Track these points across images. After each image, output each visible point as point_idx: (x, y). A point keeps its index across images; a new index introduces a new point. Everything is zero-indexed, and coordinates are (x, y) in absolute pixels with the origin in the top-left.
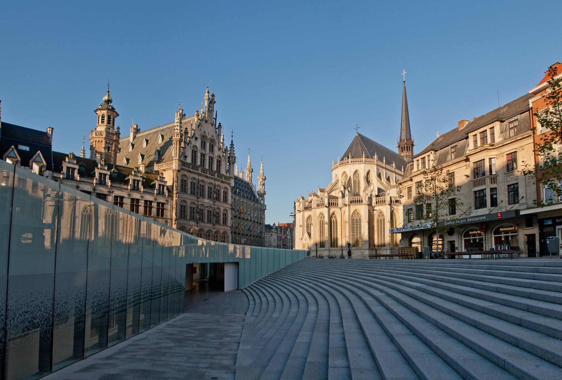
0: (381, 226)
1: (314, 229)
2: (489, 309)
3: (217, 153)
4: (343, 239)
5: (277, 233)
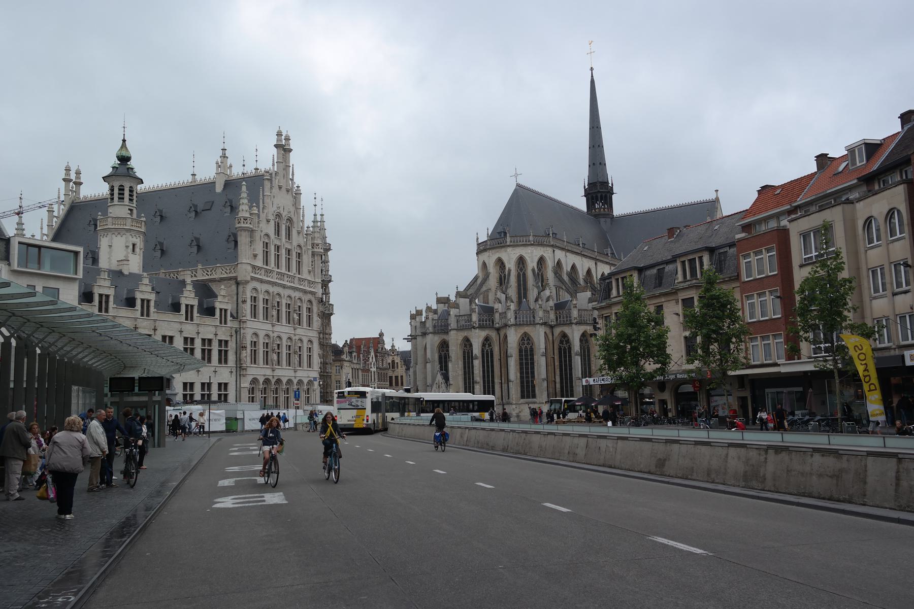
0: (565, 361)
2: (102, 425)
3: (296, 239)
4: (503, 385)
5: (350, 361)
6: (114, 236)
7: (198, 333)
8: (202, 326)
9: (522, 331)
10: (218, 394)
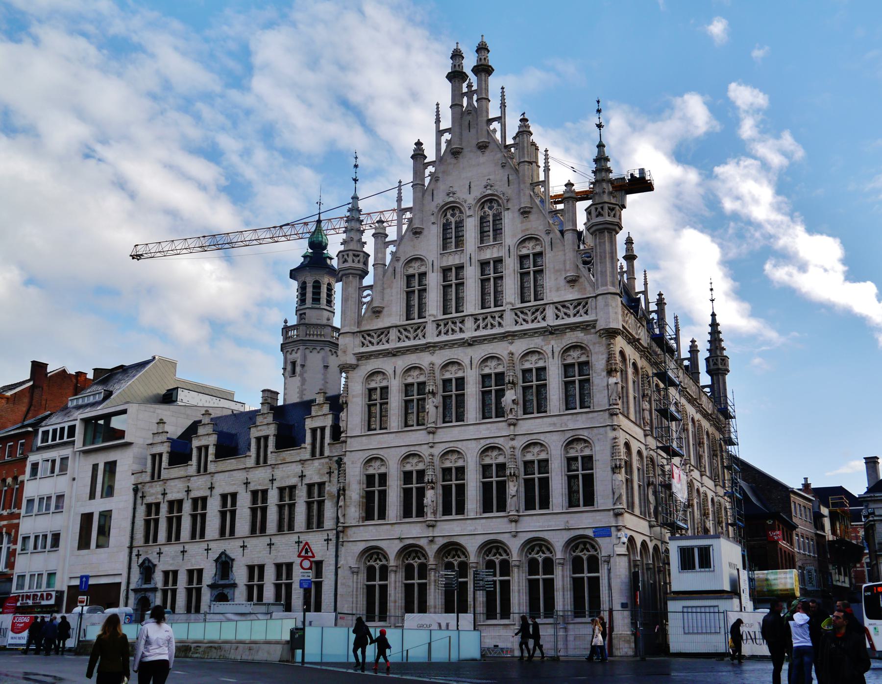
6: (307, 351)
7: (272, 480)
8: (280, 466)
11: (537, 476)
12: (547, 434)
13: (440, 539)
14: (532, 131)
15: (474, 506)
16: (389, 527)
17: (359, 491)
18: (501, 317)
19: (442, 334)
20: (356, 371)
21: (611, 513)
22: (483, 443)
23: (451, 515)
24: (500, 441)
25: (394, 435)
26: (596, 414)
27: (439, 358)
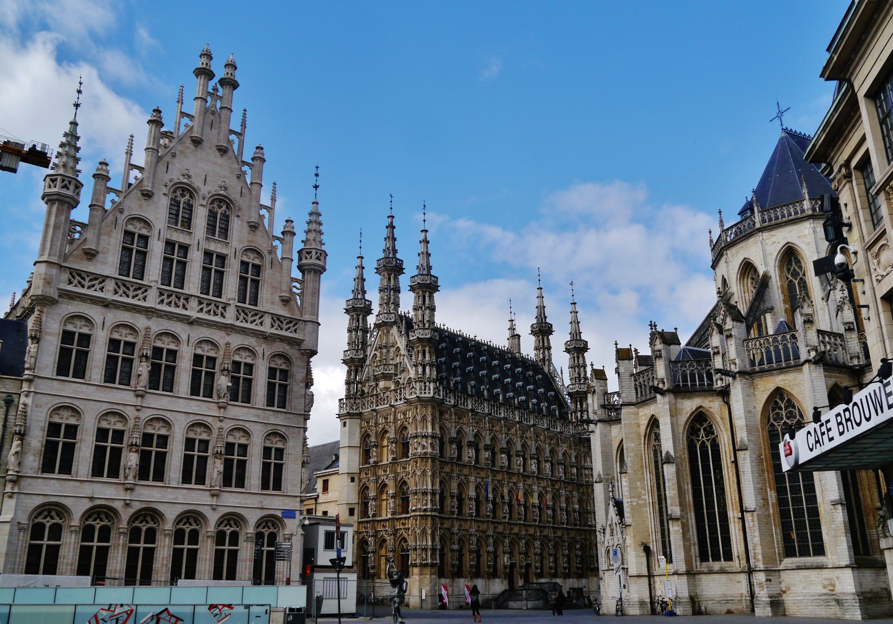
1: (632, 488)
9: (766, 386)
10: (130, 548)
11: (236, 457)
12: (252, 423)
13: (138, 503)
14: (266, 159)
15: (177, 476)
16: (78, 484)
17: (41, 439)
18: (224, 308)
19: (164, 304)
20: (54, 307)
21: (298, 499)
22: (192, 417)
23: (148, 480)
24: (210, 420)
25: (94, 388)
26: (292, 416)
27: (157, 325)
